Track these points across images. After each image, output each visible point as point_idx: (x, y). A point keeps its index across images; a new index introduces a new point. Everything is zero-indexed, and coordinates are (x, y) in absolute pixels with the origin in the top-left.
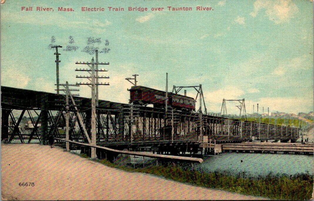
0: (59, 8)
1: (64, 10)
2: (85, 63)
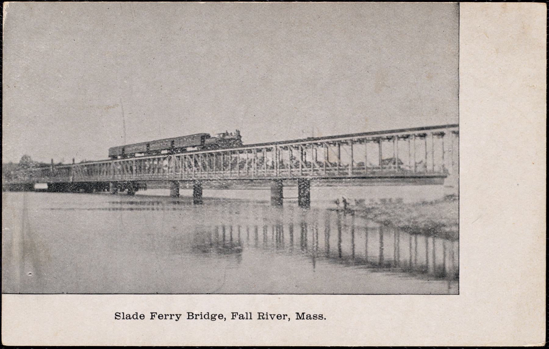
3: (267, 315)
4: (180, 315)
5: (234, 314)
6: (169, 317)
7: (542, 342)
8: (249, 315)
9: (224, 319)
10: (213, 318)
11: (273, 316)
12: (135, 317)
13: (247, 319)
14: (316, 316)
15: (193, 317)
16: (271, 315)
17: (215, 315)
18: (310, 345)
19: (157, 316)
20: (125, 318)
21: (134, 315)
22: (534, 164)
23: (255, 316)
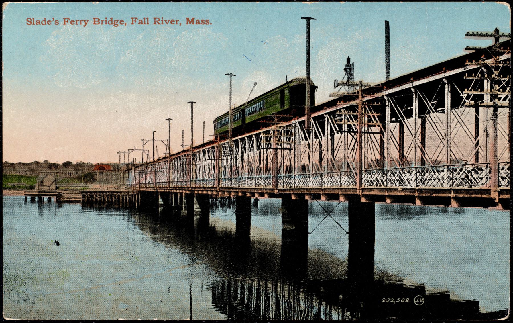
0: (188, 19)
1: (37, 24)
2: (505, 34)
3: (162, 21)
4: (88, 21)
5: (134, 19)
6: (79, 23)
7: (6, 5)
8: (146, 20)
9: (124, 25)
10: (115, 24)
11: (167, 21)
12: (110, 22)
13: (145, 24)
14: (28, 22)
15: (99, 23)
16: (166, 21)
17: (117, 21)
18: (246, 3)
19: (69, 21)
20: (35, 23)
21: (42, 21)
22: (256, 84)
23: (151, 21)
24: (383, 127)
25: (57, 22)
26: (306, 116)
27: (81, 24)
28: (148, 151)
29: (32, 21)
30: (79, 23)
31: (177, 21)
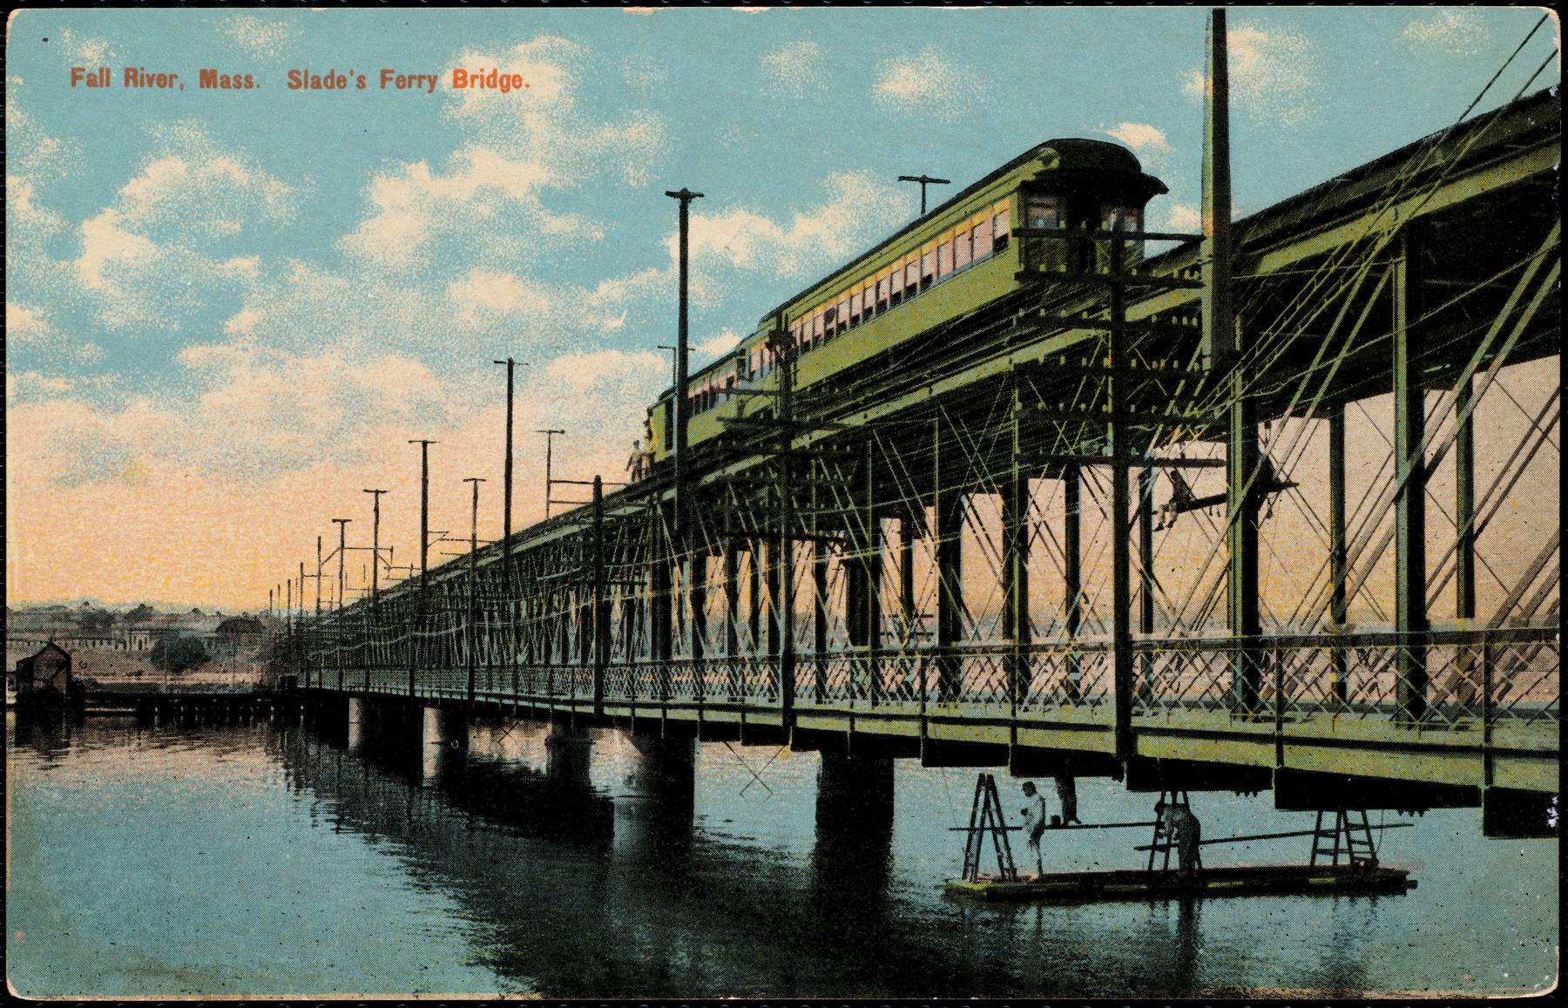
2: (1521, 722)
15: (466, 82)
24: (1293, 394)
25: (131, 76)
26: (11, 665)
27: (420, 86)
28: (511, 364)
29: (302, 78)
30: (415, 82)
31: (171, 77)
